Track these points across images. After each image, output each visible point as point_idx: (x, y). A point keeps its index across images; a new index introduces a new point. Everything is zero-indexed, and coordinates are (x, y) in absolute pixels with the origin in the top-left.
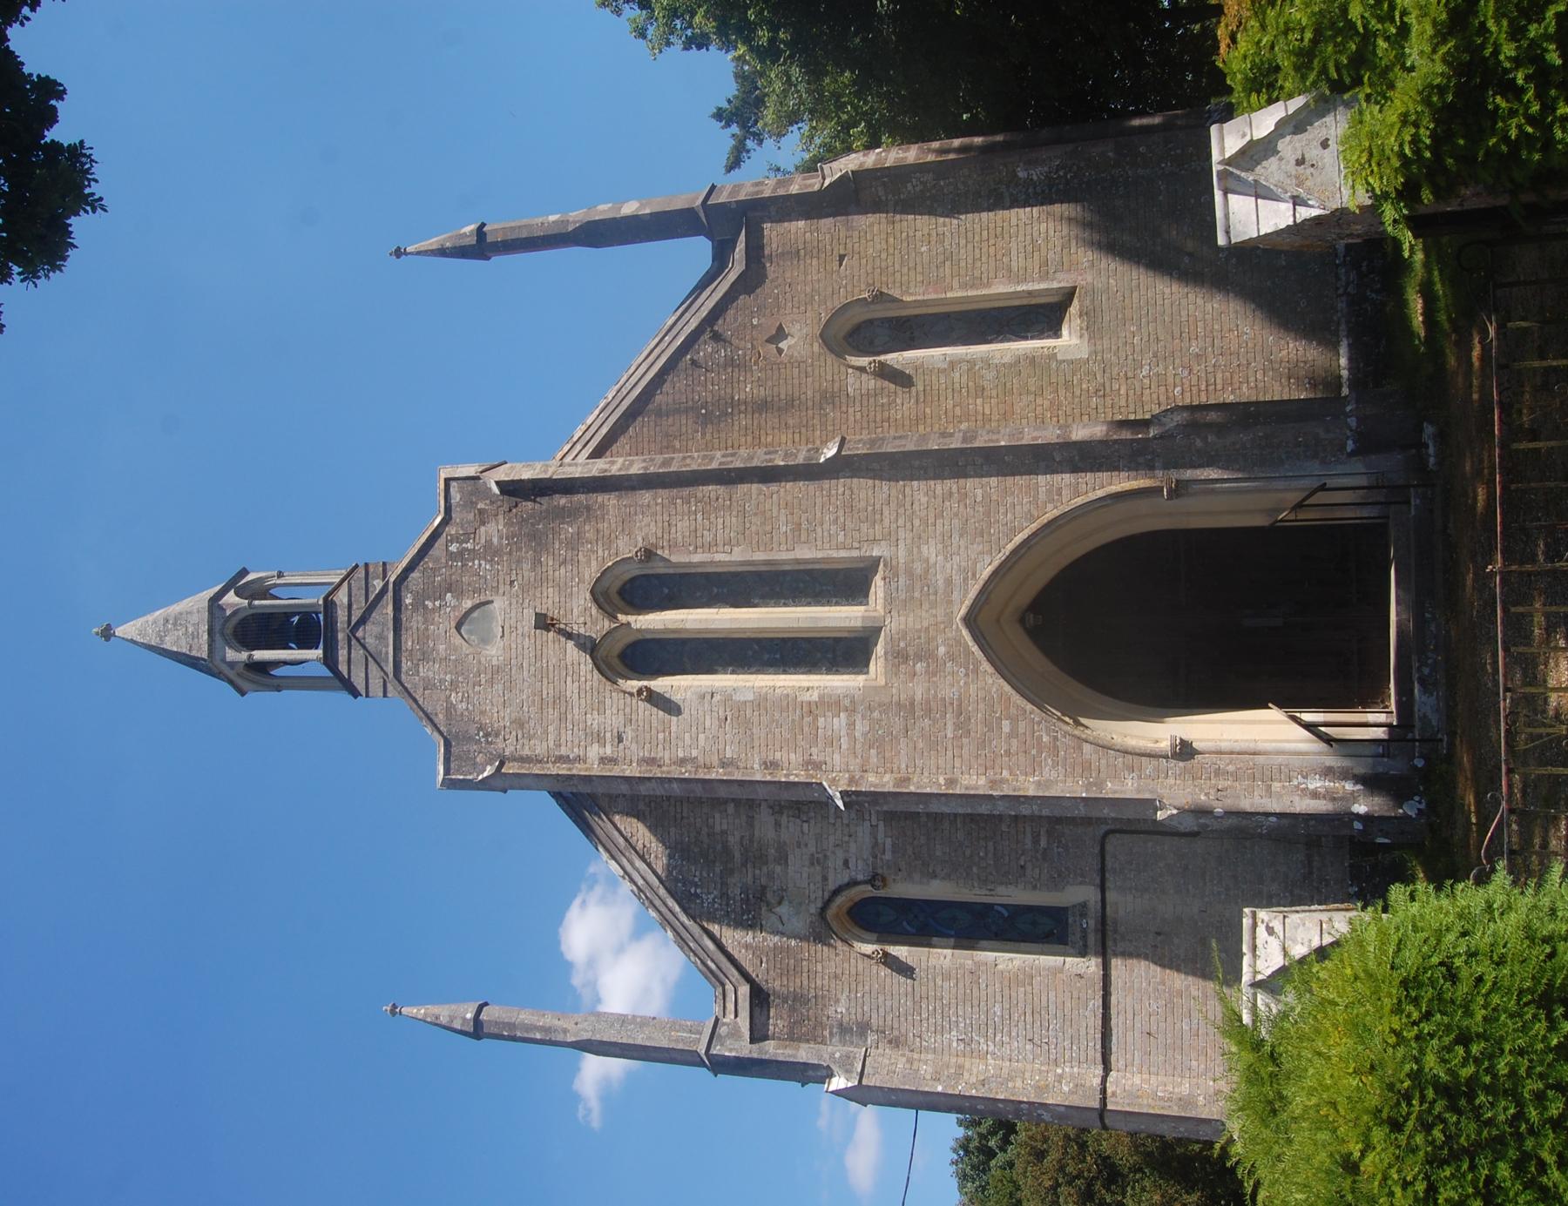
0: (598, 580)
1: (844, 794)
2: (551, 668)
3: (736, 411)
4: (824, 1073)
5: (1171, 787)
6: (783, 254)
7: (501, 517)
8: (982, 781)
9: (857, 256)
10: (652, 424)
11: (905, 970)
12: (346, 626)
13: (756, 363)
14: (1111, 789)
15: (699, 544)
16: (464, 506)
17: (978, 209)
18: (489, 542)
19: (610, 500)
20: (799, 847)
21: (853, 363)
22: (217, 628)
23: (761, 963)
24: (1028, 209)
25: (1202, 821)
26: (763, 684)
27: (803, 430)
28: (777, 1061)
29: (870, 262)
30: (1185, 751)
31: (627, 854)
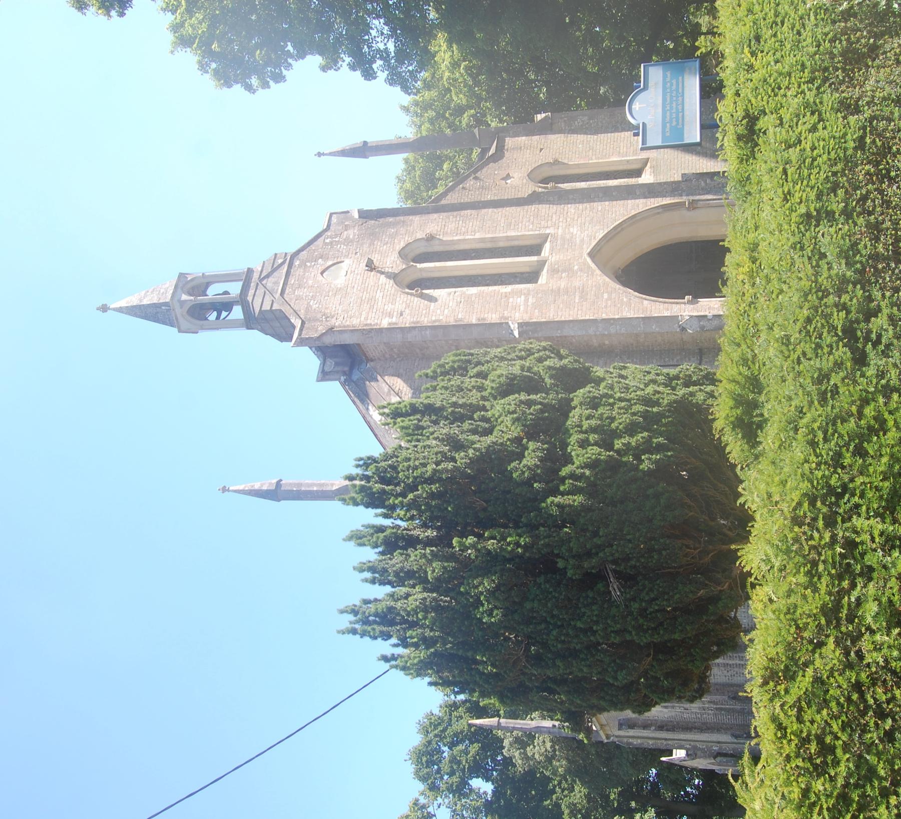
0: (403, 248)
1: (520, 325)
2: (370, 287)
7: (357, 227)
13: (495, 187)
22: (181, 285)
25: (701, 323)
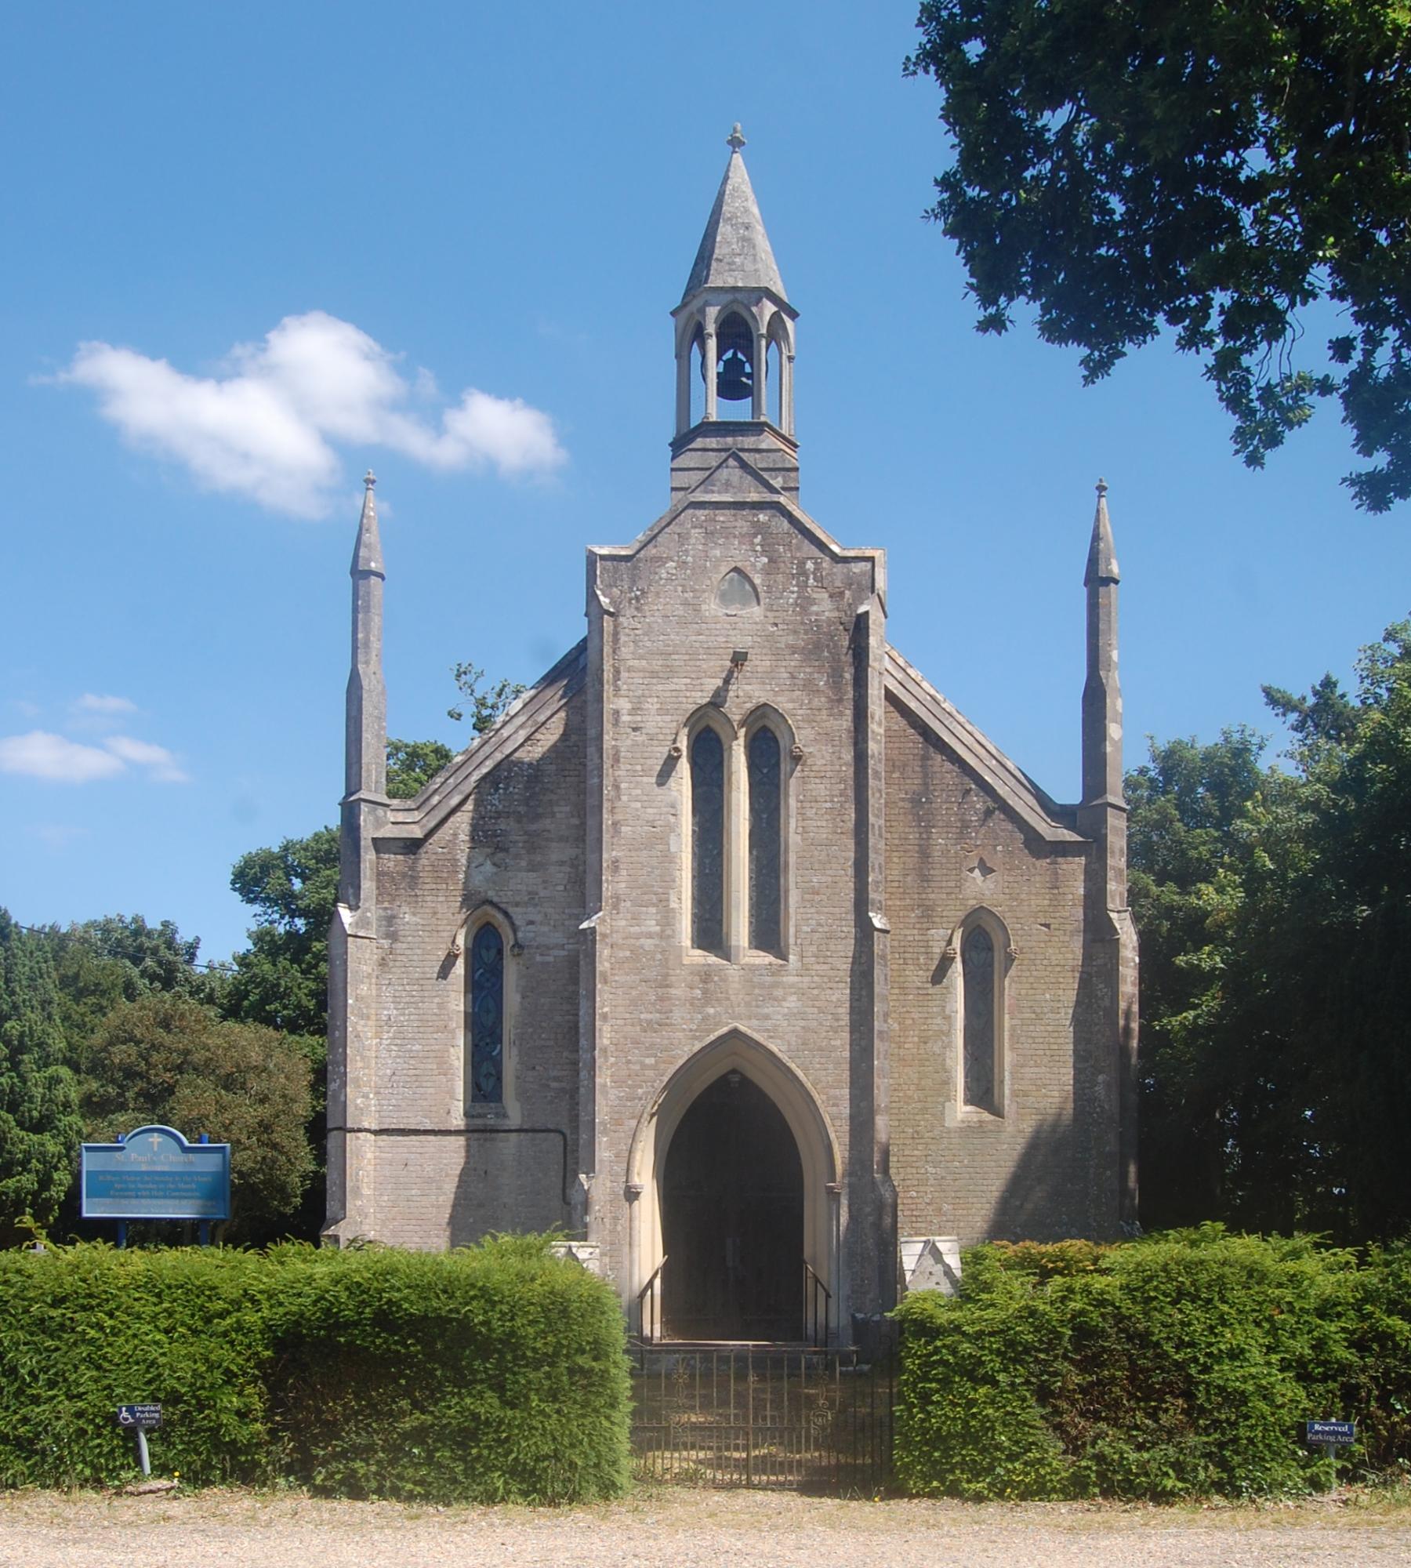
1: (593, 930)
2: (698, 663)
3: (922, 830)
4: (353, 903)
6: (1057, 874)
7: (836, 614)
8: (606, 1042)
9: (1047, 938)
10: (916, 751)
11: (444, 972)
12: (739, 446)
14: (602, 1141)
15: (805, 804)
16: (848, 577)
17: (1076, 1042)
18: (813, 602)
19: (846, 722)
20: (544, 882)
21: (955, 934)
22: (739, 296)
24: (1072, 1082)
26: (684, 859)
27: (901, 890)
28: (359, 862)
29: (1043, 950)
30: (632, 1195)
31: (530, 722)
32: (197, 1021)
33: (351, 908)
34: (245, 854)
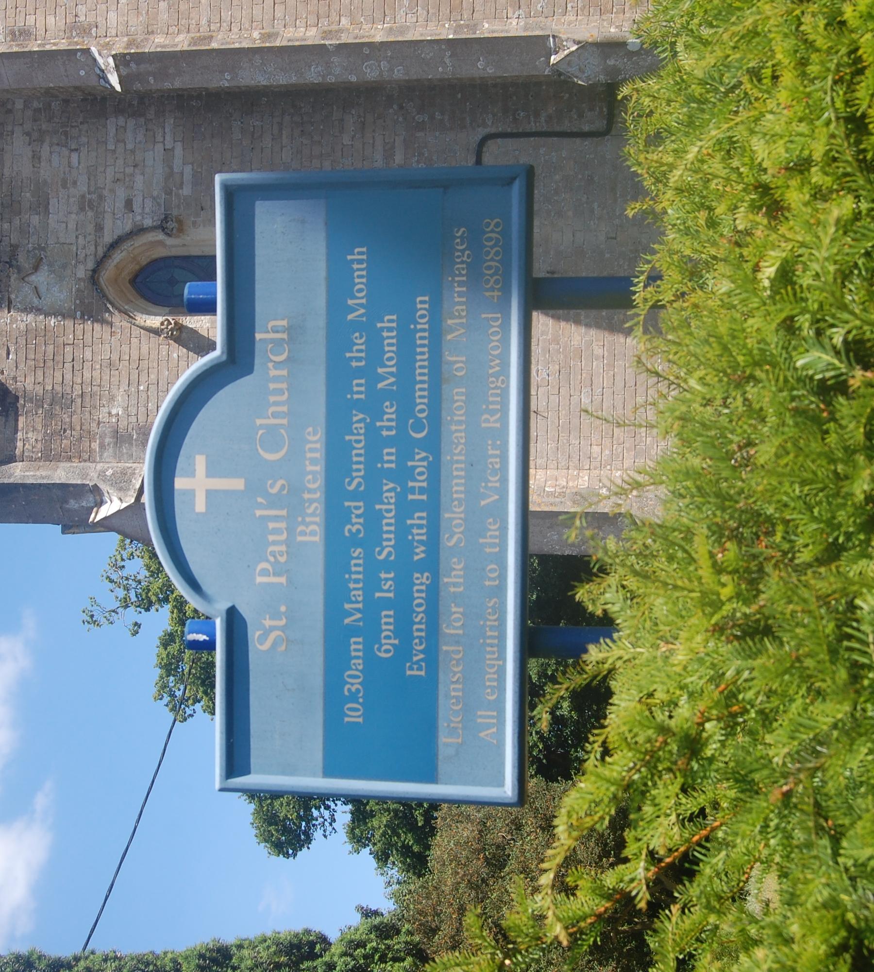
1: (121, 60)
5: (569, 23)
20: (64, 185)
23: (8, 354)
25: (611, 62)
28: (24, 486)
32: (428, 897)
33: (100, 503)
34: (256, 840)
